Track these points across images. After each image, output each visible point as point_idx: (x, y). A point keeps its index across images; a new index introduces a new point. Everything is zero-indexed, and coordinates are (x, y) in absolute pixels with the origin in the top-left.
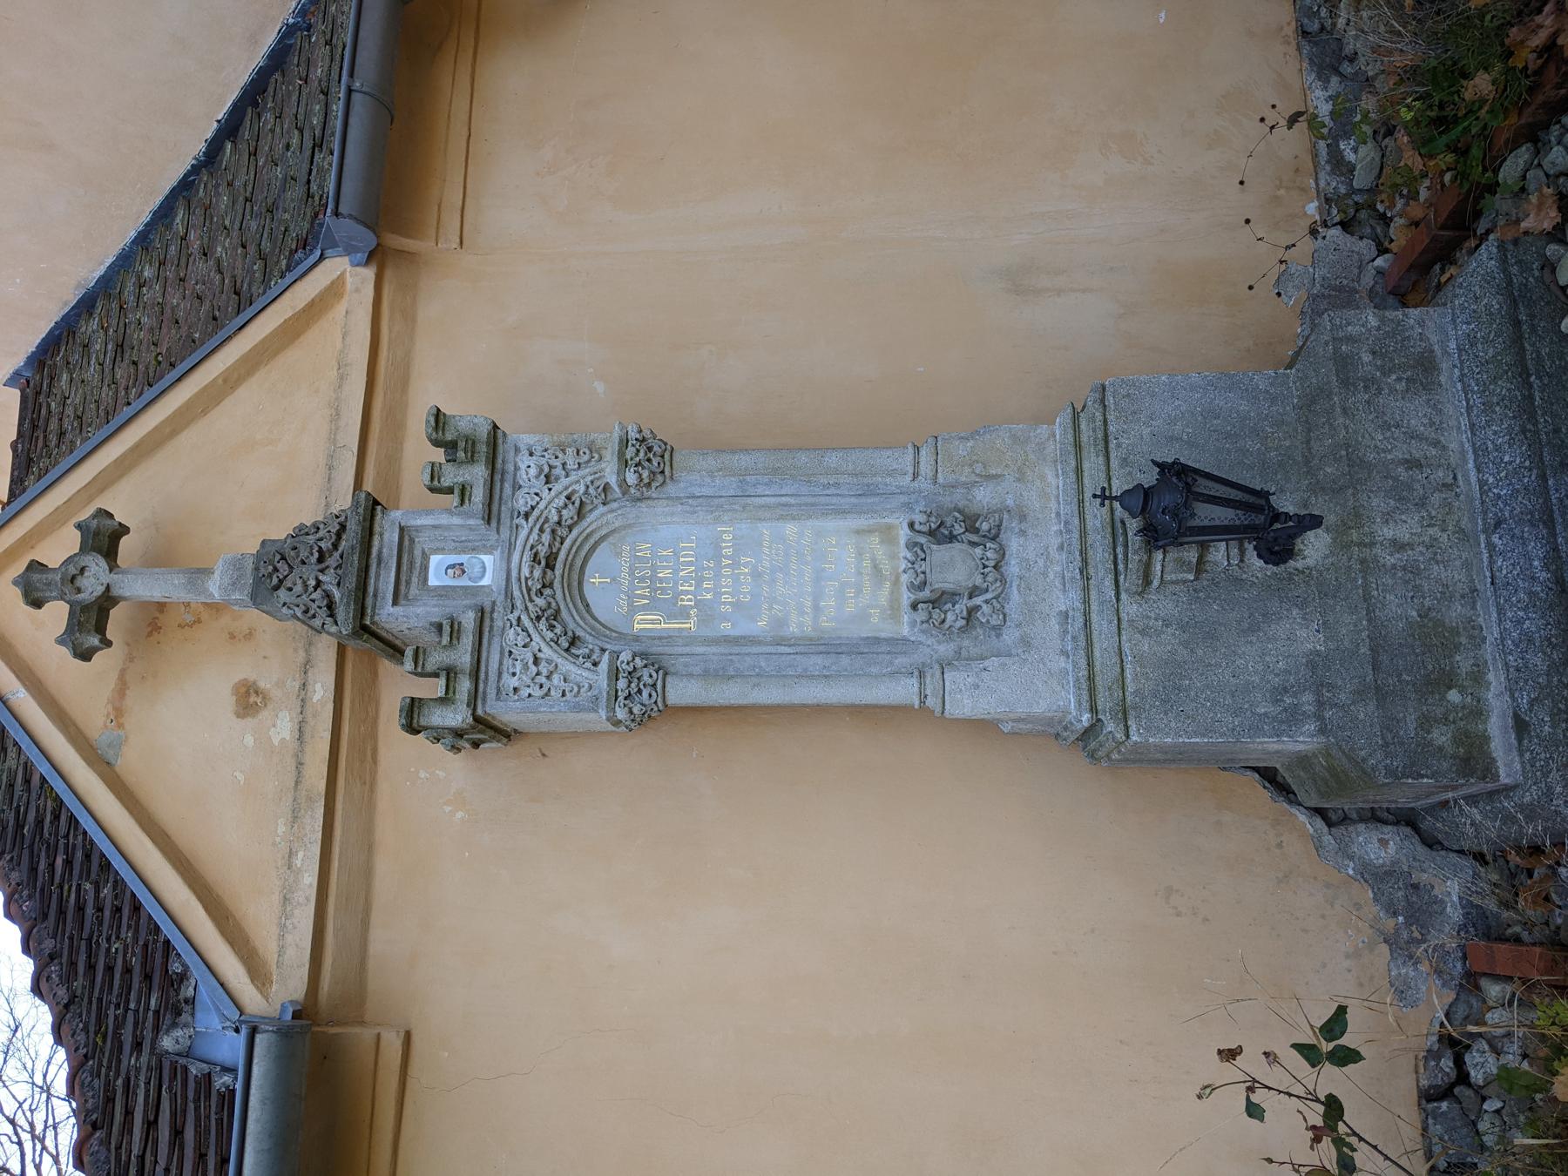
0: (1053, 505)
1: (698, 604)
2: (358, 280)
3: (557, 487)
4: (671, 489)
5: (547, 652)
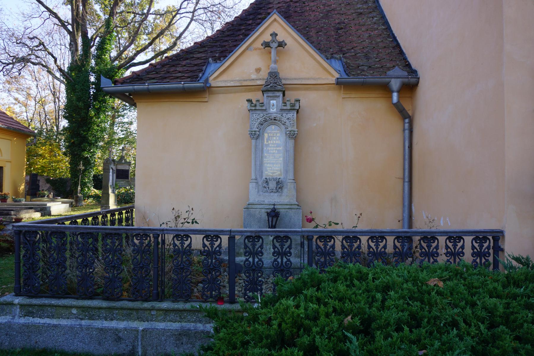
0: (282, 201)
1: (269, 144)
2: (333, 80)
3: (287, 120)
4: (288, 139)
5: (259, 120)
